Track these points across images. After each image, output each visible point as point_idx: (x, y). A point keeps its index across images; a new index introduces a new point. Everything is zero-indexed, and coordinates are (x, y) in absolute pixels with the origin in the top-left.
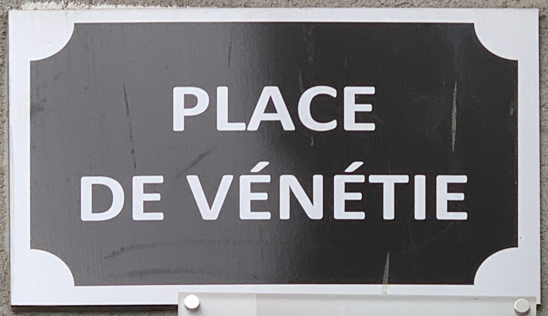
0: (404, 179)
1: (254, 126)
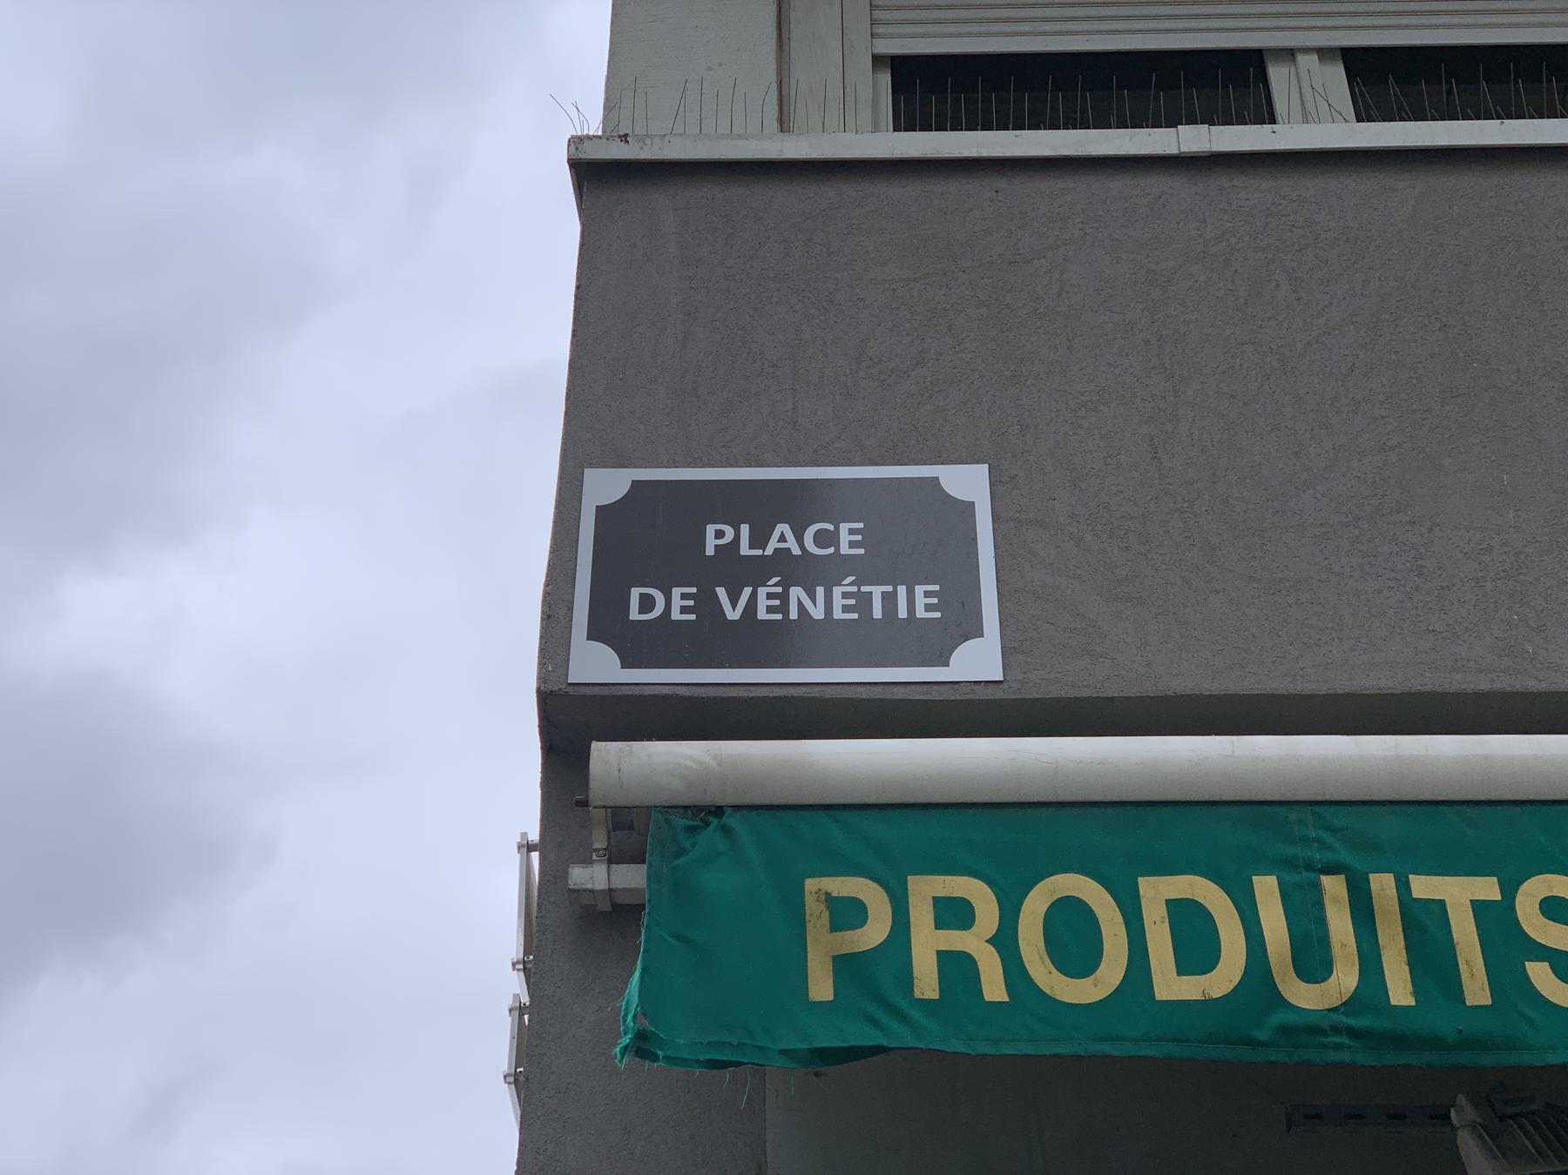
0: (890, 588)
1: (769, 551)
